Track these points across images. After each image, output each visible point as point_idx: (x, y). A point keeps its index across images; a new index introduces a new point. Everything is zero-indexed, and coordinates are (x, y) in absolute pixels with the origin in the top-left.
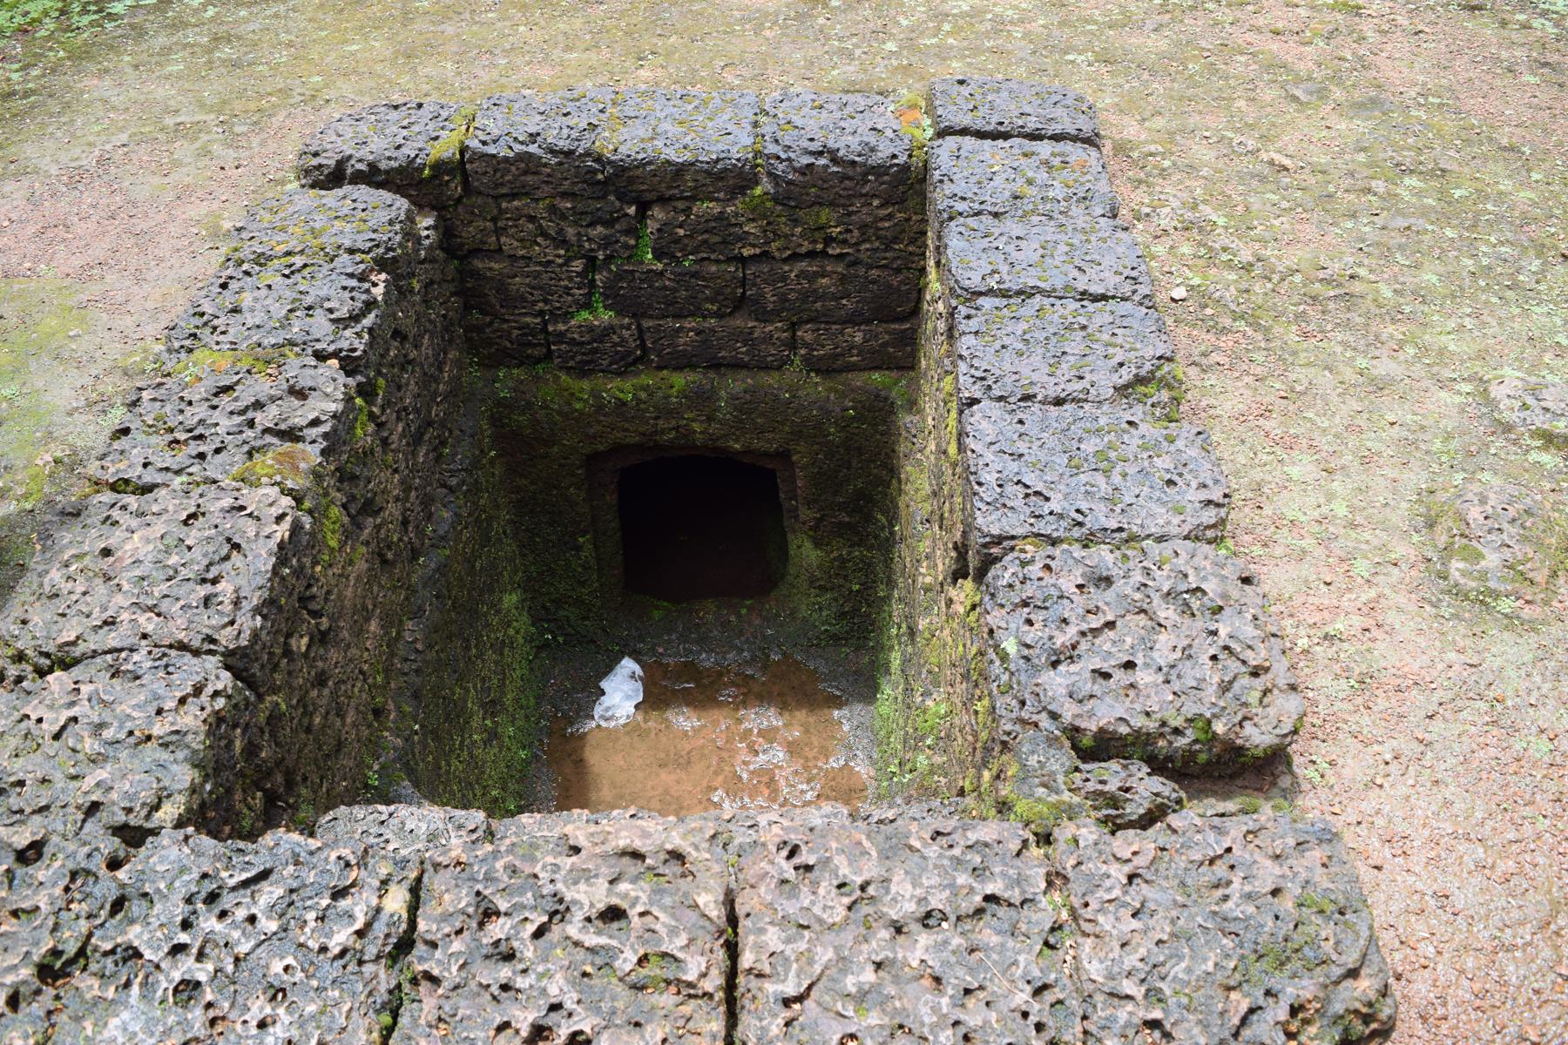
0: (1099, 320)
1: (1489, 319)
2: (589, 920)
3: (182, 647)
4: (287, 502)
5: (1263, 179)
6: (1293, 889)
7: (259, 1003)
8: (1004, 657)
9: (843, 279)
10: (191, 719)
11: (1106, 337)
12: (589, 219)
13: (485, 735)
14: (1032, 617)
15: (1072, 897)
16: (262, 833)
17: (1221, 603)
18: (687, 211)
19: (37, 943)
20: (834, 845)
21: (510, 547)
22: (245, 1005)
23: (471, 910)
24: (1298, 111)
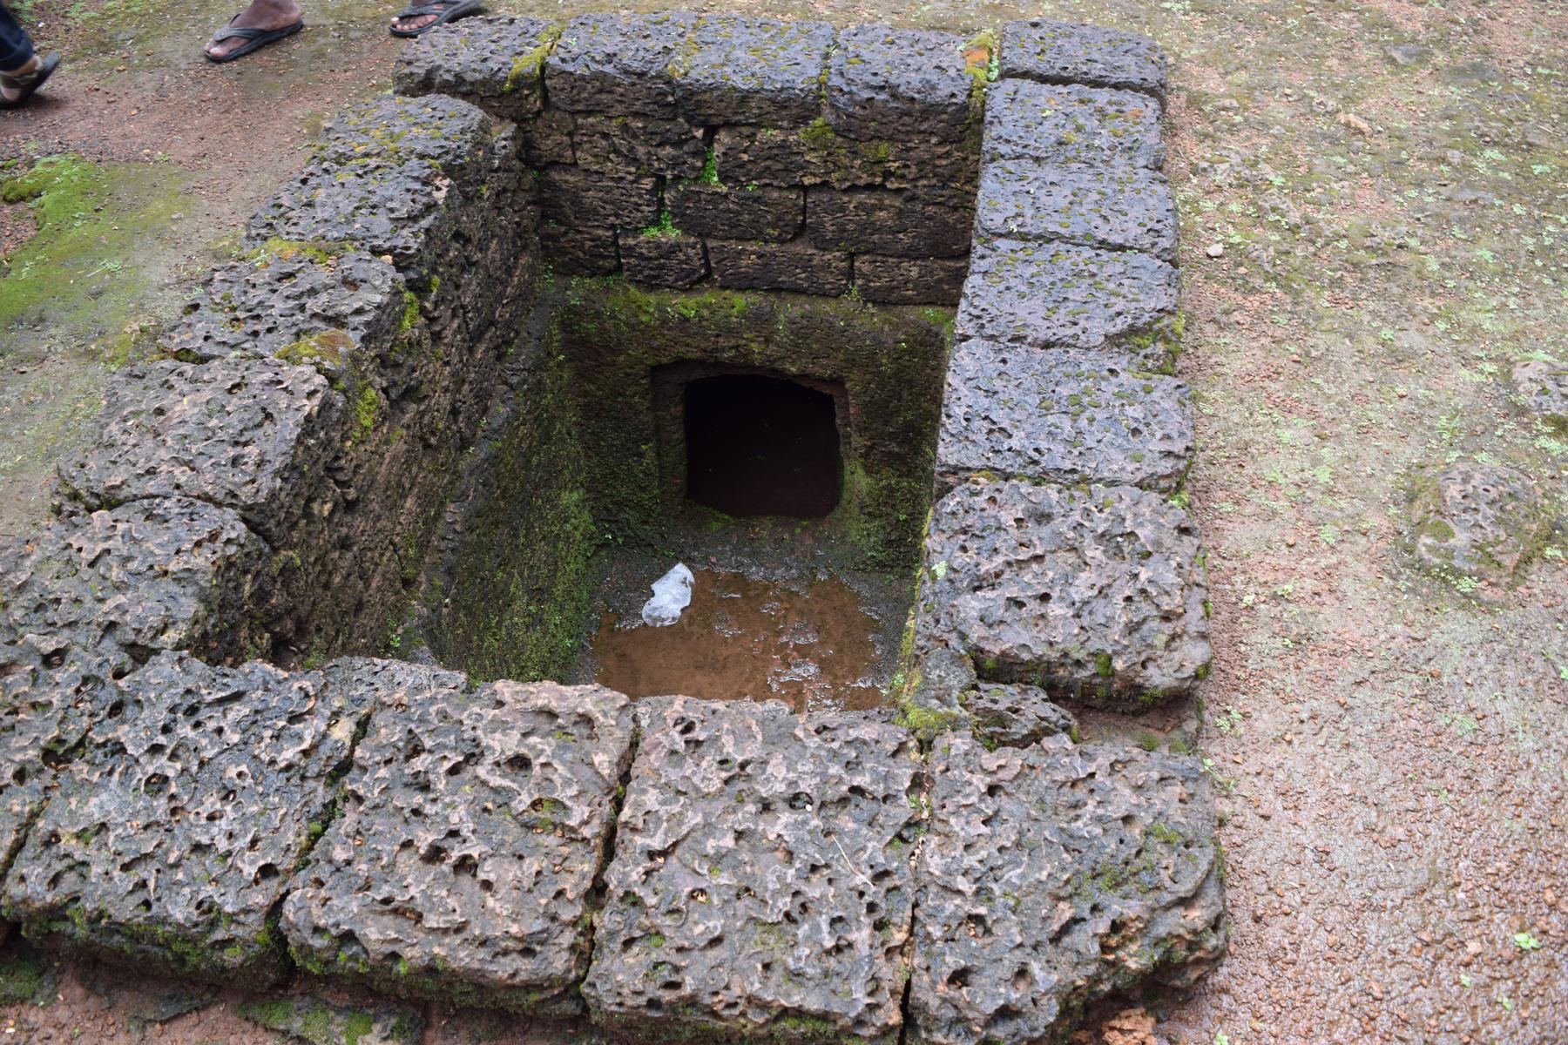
1: (1537, 301)
2: (497, 764)
3: (208, 499)
4: (320, 380)
5: (1334, 140)
9: (900, 213)
10: (202, 560)
12: (658, 139)
19: (45, 732)
20: (726, 726)
21: (574, 447)
23: (401, 744)
24: (1392, 74)
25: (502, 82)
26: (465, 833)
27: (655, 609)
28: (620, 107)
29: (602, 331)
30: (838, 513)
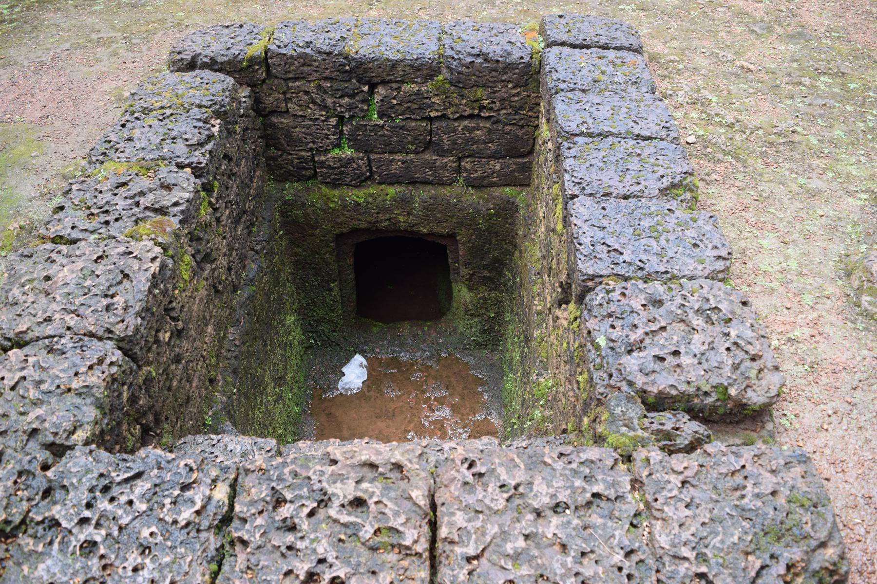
0: (647, 151)
2: (343, 506)
3: (92, 335)
4: (158, 250)
5: (737, 76)
6: (785, 492)
7: (134, 556)
8: (598, 347)
9: (490, 131)
10: (95, 379)
11: (652, 160)
12: (340, 93)
13: (275, 397)
14: (614, 323)
15: (647, 495)
16: (139, 449)
17: (730, 316)
18: (398, 89)
20: (497, 461)
21: (291, 288)
22: (125, 557)
24: (756, 39)
25: (241, 62)
26: (330, 559)
27: (347, 383)
28: (316, 75)
29: (306, 215)
30: (450, 316)
